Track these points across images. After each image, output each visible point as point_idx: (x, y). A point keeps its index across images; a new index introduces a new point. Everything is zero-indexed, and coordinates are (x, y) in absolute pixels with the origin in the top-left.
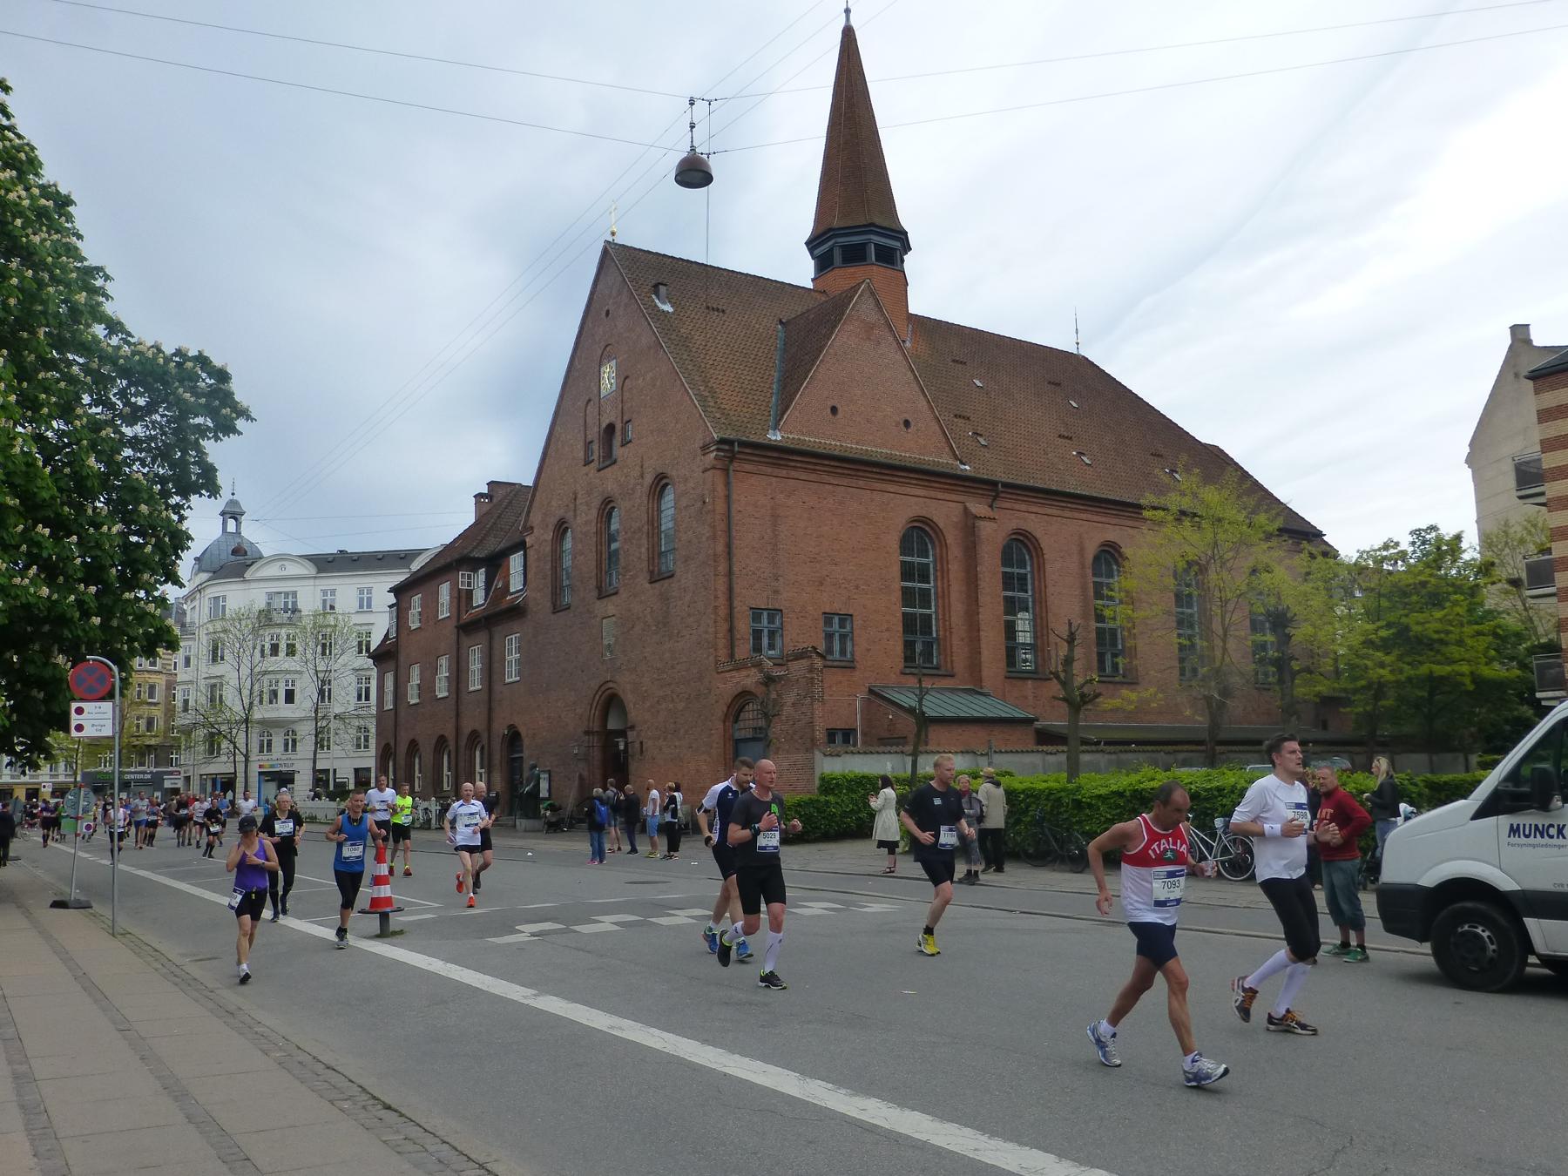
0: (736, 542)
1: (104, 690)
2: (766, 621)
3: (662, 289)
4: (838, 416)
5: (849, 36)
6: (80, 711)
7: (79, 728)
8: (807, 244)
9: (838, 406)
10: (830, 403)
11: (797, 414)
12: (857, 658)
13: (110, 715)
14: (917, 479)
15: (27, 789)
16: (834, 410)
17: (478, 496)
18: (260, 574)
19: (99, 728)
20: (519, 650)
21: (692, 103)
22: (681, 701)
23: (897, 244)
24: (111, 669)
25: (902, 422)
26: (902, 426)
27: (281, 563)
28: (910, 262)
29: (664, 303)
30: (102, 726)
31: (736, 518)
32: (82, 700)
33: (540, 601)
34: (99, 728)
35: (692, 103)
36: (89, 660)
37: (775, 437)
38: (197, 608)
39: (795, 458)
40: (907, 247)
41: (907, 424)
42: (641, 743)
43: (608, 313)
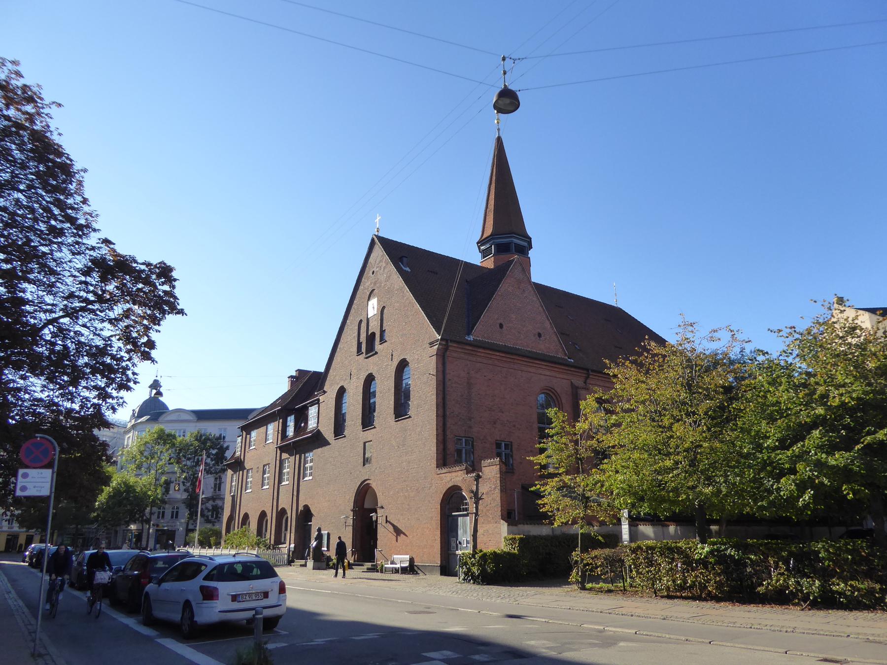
0: (448, 397)
1: (46, 462)
2: (464, 444)
3: (405, 259)
4: (503, 329)
5: (499, 140)
6: (25, 476)
7: (24, 488)
8: (478, 243)
9: (503, 324)
10: (499, 322)
11: (481, 327)
12: (515, 468)
13: (49, 479)
14: (546, 365)
15: (27, 535)
16: (501, 326)
17: (291, 377)
18: (166, 419)
19: (39, 489)
20: (72, 561)
21: (504, 59)
22: (412, 492)
23: (525, 244)
24: (52, 443)
25: (537, 334)
26: (537, 336)
27: (179, 413)
28: (531, 253)
29: (405, 267)
30: (41, 487)
31: (448, 383)
32: (27, 467)
33: (328, 432)
34: (39, 489)
35: (504, 59)
36: (37, 437)
37: (471, 338)
38: (131, 438)
39: (480, 350)
40: (531, 247)
41: (540, 335)
42: (386, 517)
43: (373, 273)
